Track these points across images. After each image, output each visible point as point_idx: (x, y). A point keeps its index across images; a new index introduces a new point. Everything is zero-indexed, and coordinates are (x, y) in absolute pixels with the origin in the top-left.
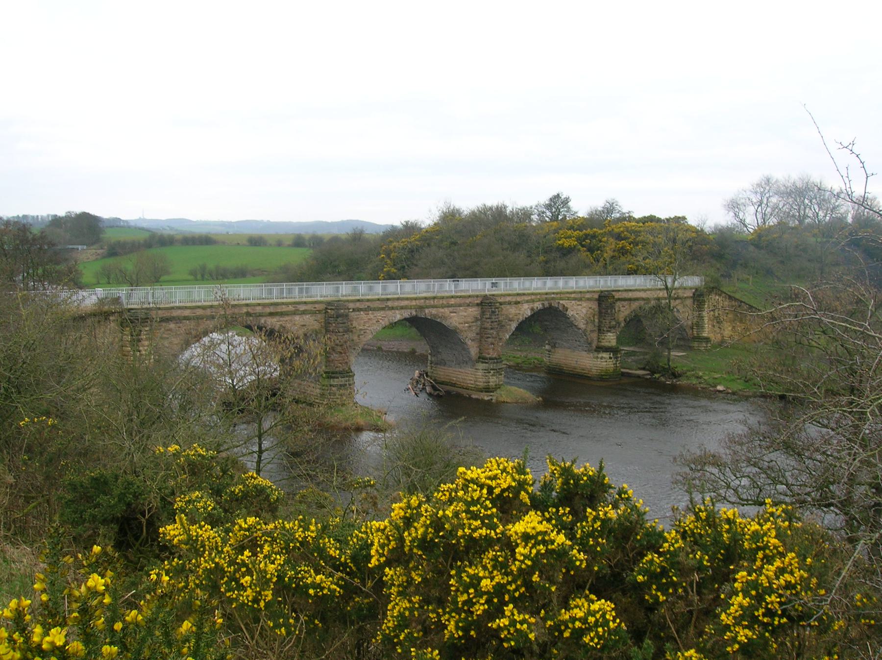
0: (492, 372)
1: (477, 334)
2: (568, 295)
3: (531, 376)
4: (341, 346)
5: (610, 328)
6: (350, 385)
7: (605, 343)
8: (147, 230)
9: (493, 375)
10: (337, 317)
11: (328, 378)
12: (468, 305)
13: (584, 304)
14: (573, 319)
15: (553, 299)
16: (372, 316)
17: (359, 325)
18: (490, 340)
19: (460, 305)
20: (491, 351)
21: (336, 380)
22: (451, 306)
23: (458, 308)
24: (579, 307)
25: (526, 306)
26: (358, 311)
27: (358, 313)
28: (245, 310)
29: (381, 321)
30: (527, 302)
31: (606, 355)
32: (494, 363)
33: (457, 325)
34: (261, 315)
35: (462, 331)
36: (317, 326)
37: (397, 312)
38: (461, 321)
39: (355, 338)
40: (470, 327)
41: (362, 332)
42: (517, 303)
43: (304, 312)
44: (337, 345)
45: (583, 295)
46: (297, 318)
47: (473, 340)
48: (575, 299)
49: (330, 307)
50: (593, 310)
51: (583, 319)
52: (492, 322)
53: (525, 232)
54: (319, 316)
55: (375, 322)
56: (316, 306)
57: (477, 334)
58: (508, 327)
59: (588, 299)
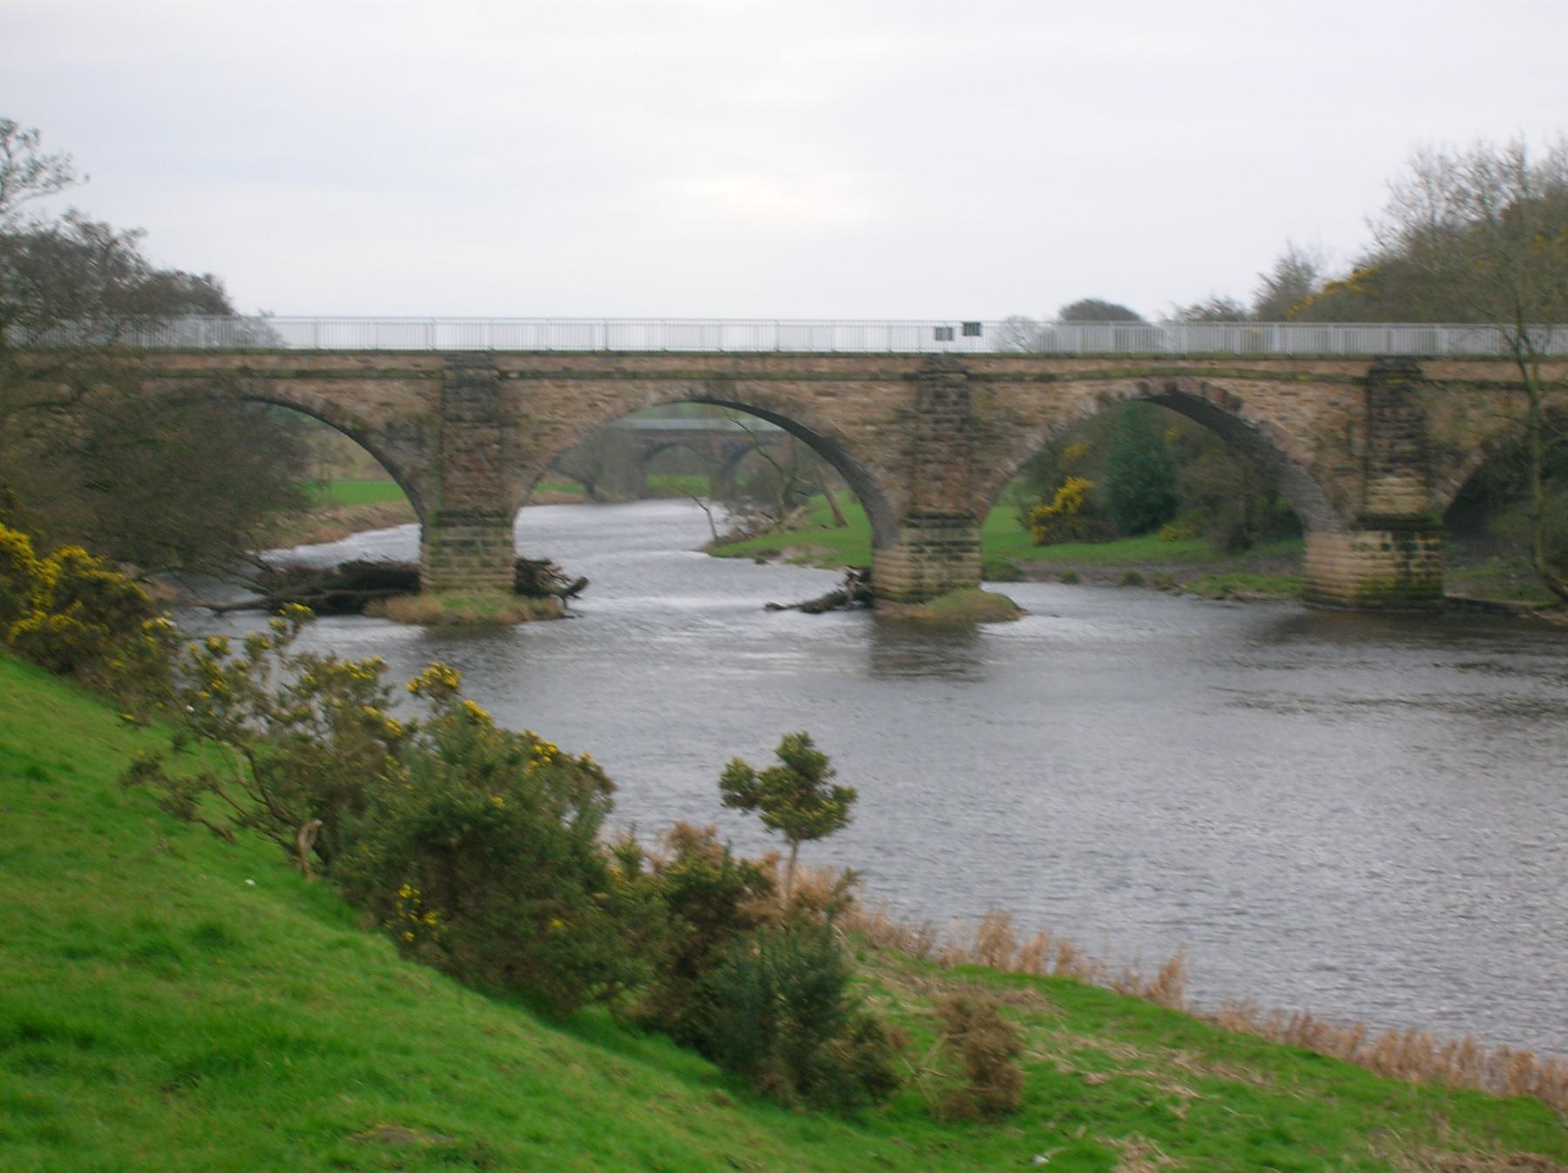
0: (928, 549)
1: (905, 453)
2: (1242, 365)
3: (1463, 723)
4: (469, 451)
5: (1391, 460)
6: (486, 544)
7: (1378, 507)
8: (1097, 586)
9: (930, 559)
10: (460, 386)
12: (875, 378)
13: (1310, 392)
14: (1268, 434)
15: (1180, 372)
18: (930, 468)
19: (847, 377)
20: (934, 497)
22: (819, 377)
23: (842, 384)
24: (1289, 401)
25: (1080, 388)
28: (237, 362)
30: (1083, 377)
31: (1371, 539)
32: (935, 526)
33: (840, 427)
34: (275, 375)
35: (853, 443)
36: (420, 407)
37: (649, 384)
38: (854, 416)
39: (526, 441)
40: (880, 433)
42: (1047, 378)
43: (386, 375)
44: (458, 450)
45: (1301, 366)
46: (370, 387)
47: (891, 469)
48: (1268, 376)
50: (1347, 409)
51: (1305, 433)
52: (937, 422)
54: (428, 384)
55: (583, 405)
56: (421, 361)
57: (905, 453)
58: (1014, 441)
59: (1323, 379)
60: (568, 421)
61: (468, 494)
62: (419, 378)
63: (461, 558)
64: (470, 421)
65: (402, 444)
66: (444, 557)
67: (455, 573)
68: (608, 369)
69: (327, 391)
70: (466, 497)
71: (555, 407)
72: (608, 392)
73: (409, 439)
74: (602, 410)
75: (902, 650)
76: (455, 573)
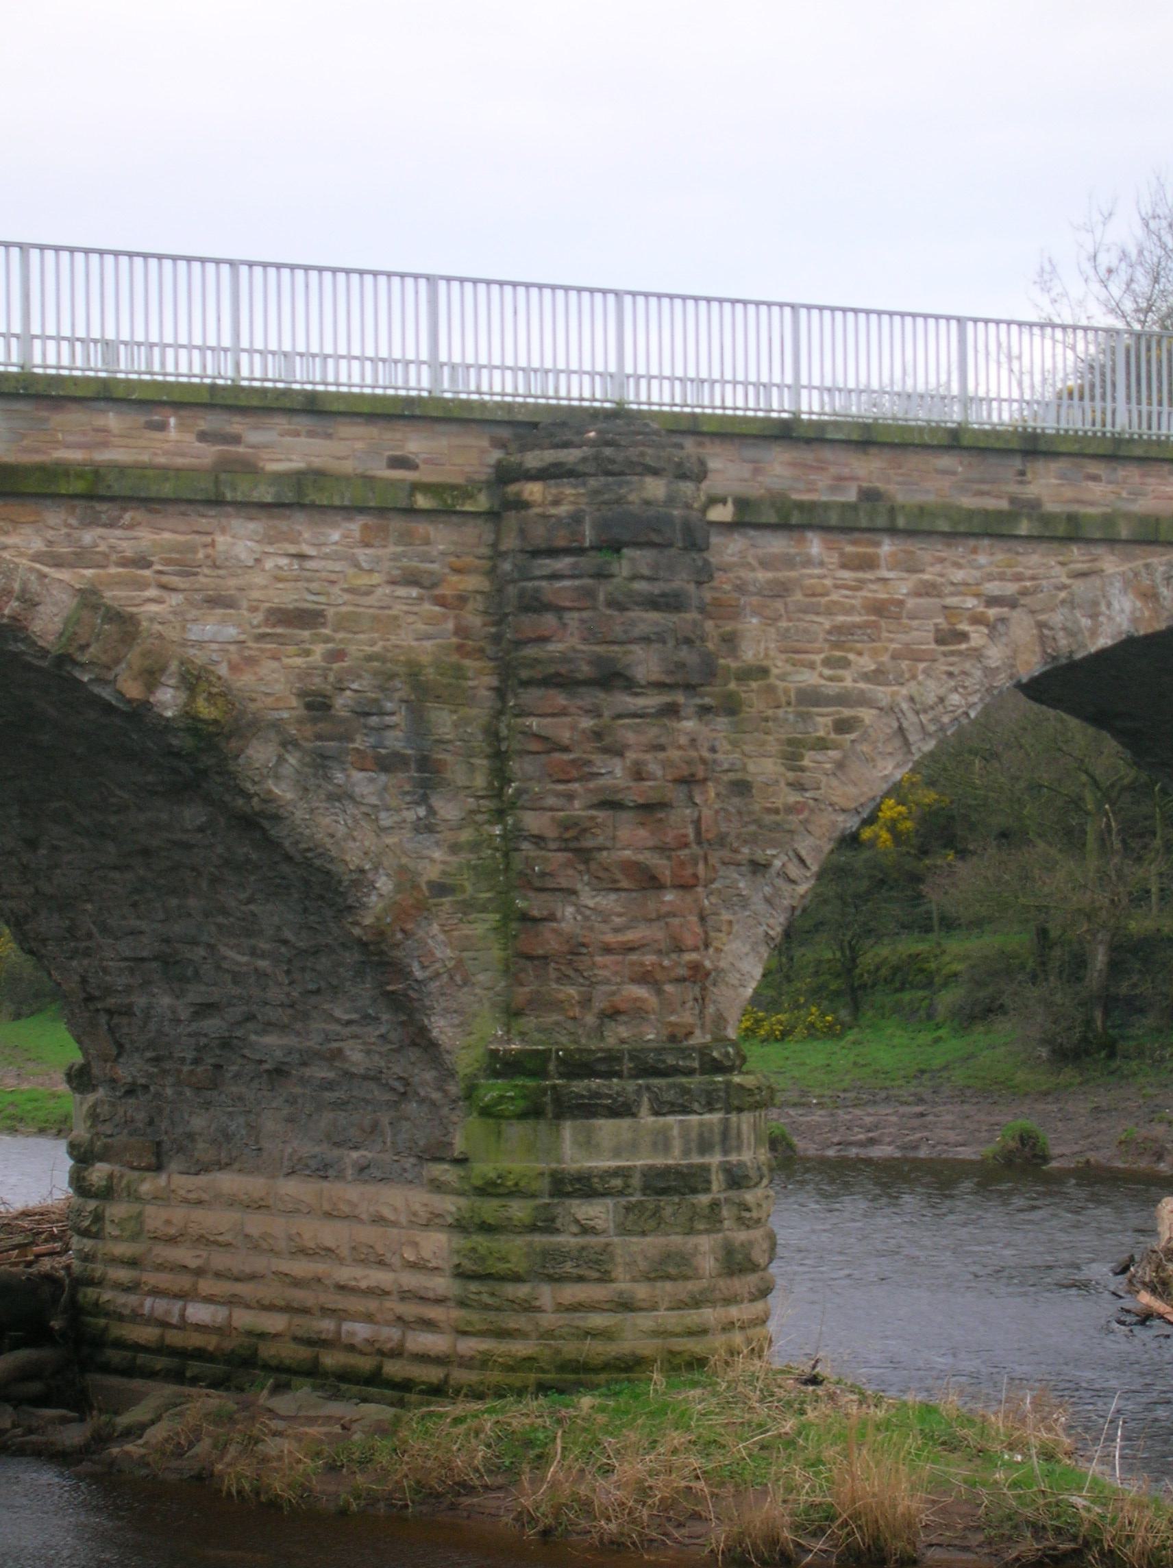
4: (650, 809)
11: (534, 1112)
16: (902, 586)
17: (794, 651)
21: (606, 1128)
26: (783, 526)
27: (777, 544)
29: (977, 636)
37: (1111, 564)
41: (822, 724)
44: (612, 804)
49: (533, 460)
53: (446, 1056)
55: (922, 635)
56: (416, 444)
60: (882, 693)
61: (645, 978)
62: (411, 511)
63: (650, 1245)
64: (660, 686)
65: (363, 783)
66: (567, 1240)
67: (626, 1305)
68: (991, 504)
69: (80, 558)
70: (641, 992)
71: (842, 636)
72: (993, 588)
73: (386, 764)
74: (977, 654)
75: (734, 1143)
76: (626, 1305)
